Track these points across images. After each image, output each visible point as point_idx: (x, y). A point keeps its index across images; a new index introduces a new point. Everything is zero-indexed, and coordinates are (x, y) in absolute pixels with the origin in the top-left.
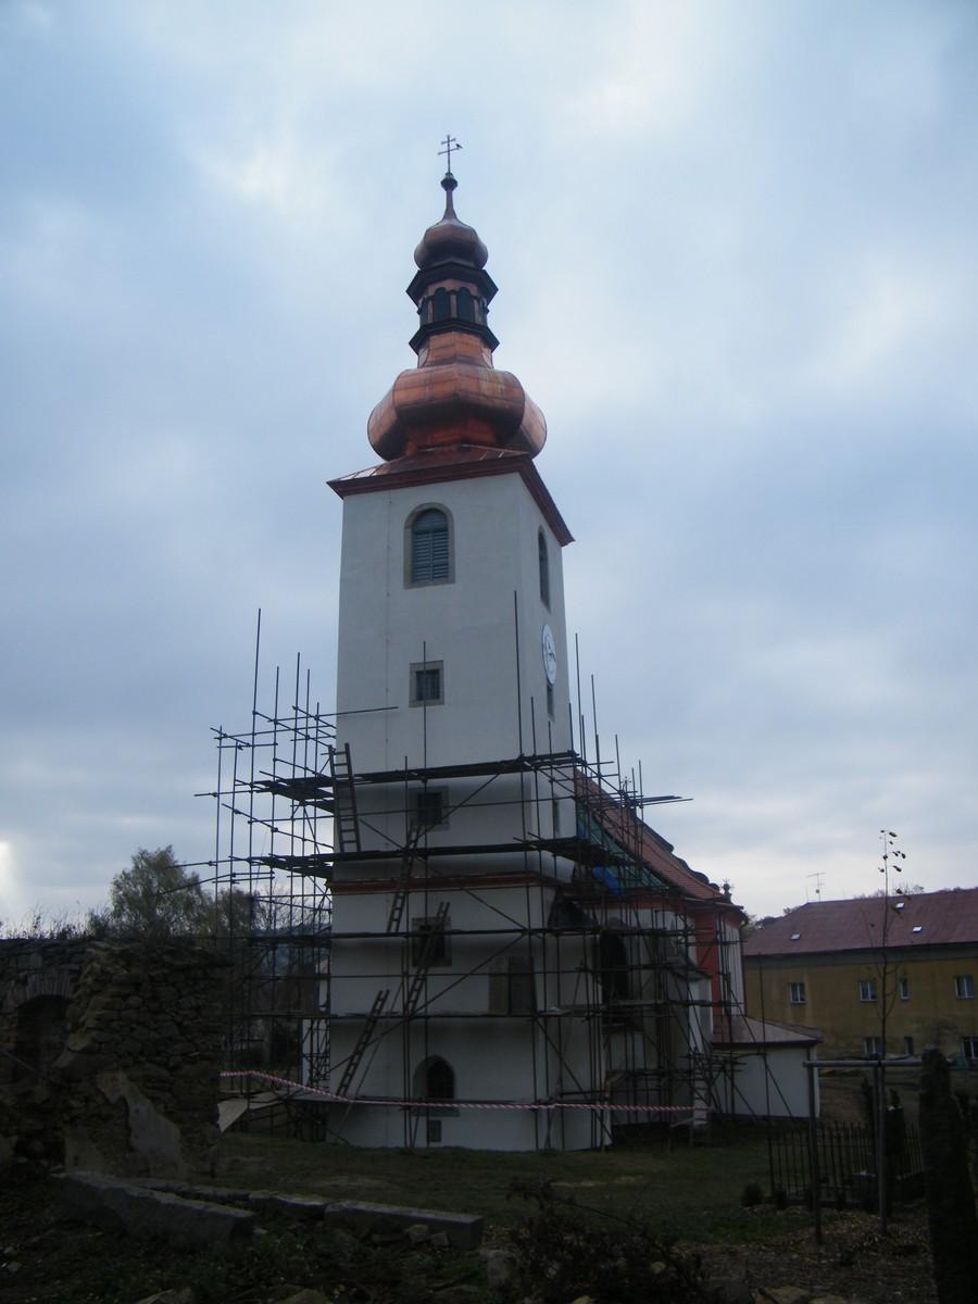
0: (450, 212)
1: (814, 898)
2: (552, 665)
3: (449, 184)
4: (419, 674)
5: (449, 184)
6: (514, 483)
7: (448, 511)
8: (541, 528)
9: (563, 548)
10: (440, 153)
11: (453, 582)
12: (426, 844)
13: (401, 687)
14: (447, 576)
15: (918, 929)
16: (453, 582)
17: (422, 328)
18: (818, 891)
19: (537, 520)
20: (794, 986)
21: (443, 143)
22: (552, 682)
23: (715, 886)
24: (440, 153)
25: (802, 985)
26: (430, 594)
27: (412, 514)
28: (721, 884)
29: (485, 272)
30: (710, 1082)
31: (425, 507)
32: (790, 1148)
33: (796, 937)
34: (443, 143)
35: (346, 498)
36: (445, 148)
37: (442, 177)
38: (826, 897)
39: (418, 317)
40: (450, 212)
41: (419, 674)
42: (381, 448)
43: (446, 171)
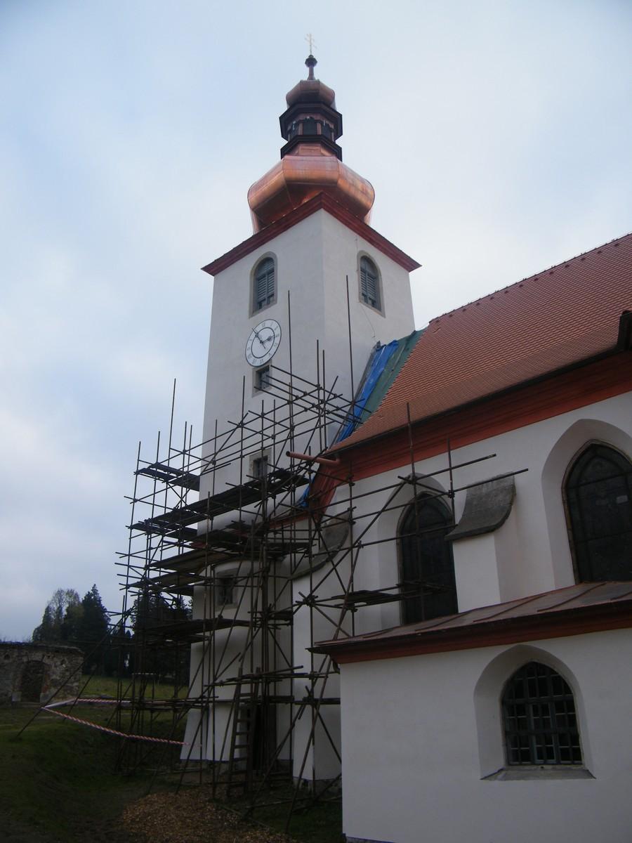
3: (311, 62)
5: (311, 62)
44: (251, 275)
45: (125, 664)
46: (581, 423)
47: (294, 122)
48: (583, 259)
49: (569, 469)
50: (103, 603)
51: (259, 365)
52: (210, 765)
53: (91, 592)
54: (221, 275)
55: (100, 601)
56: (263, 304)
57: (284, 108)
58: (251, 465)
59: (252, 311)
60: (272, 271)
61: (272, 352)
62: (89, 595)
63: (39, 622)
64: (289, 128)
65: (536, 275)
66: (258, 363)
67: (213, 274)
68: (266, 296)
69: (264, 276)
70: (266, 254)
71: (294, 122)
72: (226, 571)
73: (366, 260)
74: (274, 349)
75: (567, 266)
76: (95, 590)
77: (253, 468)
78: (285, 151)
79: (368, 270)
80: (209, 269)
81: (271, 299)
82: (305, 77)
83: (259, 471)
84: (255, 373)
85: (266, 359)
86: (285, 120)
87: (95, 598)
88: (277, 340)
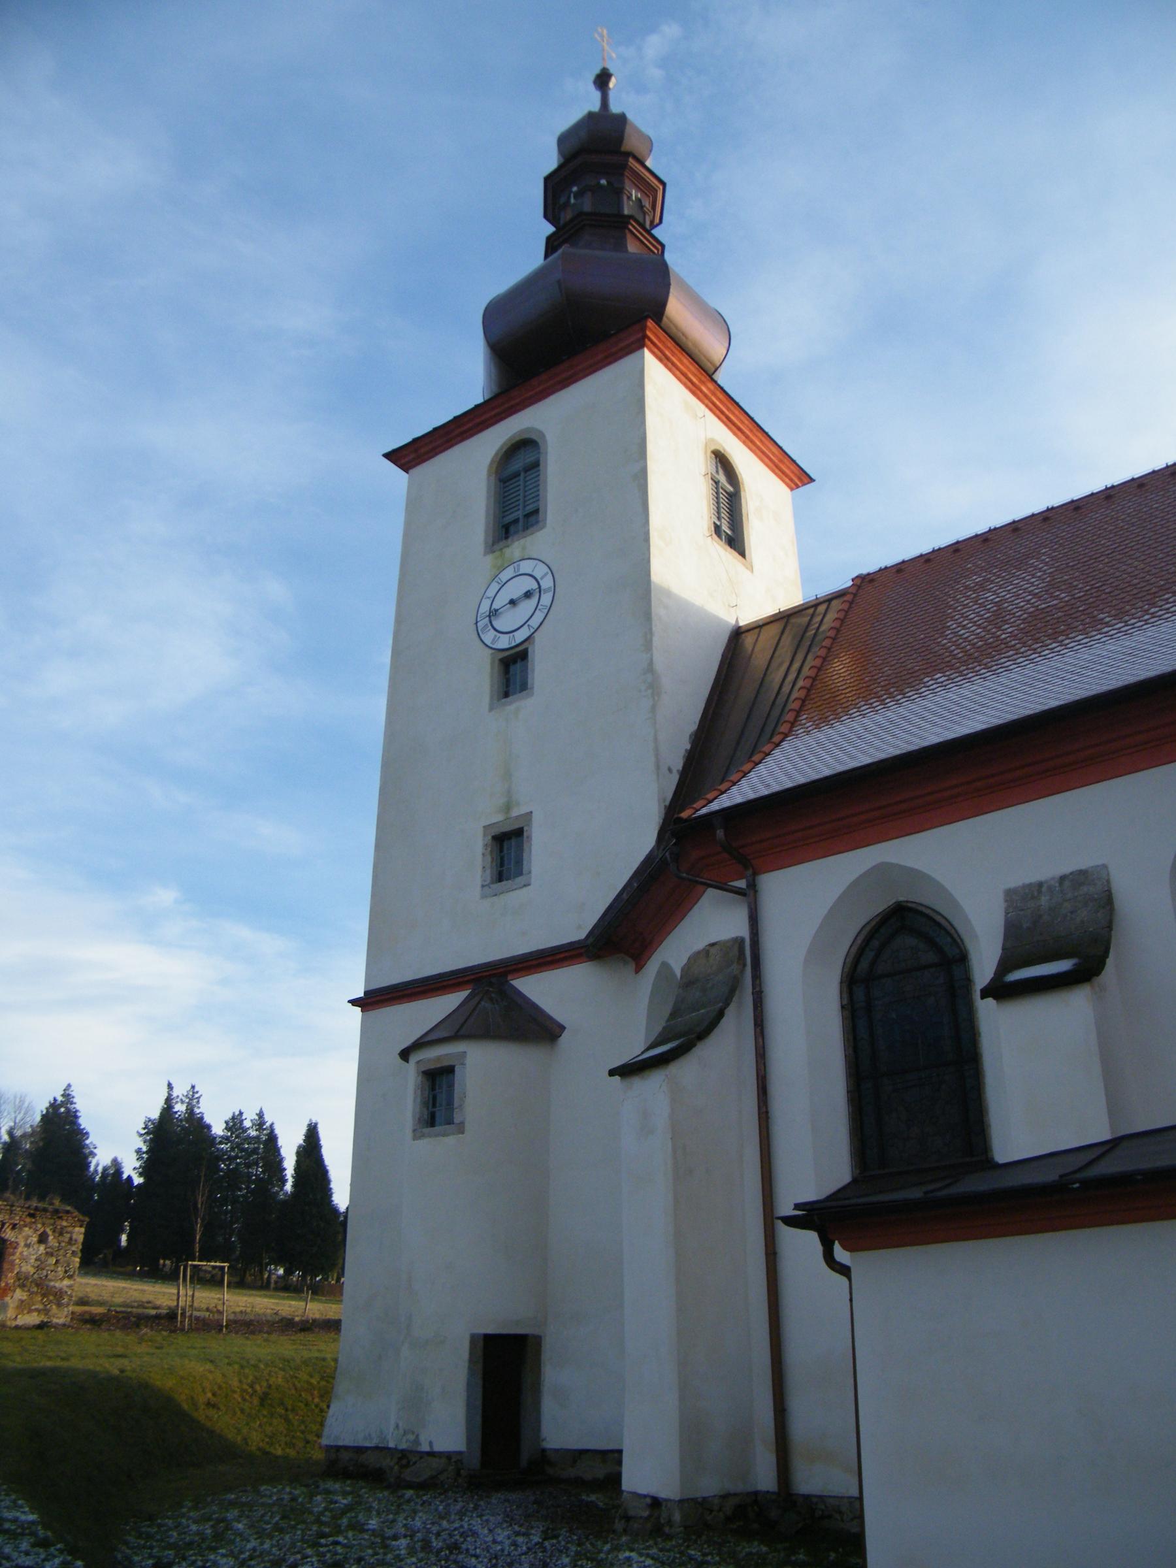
3: (602, 80)
5: (602, 80)
44: (489, 471)
45: (120, 1241)
46: (882, 871)
47: (575, 189)
48: (957, 551)
49: (854, 950)
50: (81, 1121)
51: (506, 646)
52: (400, 1459)
53: (60, 1099)
54: (413, 471)
55: (77, 1117)
56: (512, 529)
57: (551, 162)
58: (486, 845)
59: (490, 542)
60: (535, 466)
61: (535, 622)
62: (54, 1106)
63: (155, 1115)
64: (562, 200)
65: (1014, 522)
66: (504, 642)
67: (406, 468)
68: (520, 514)
69: (516, 475)
70: (523, 431)
71: (575, 189)
72: (439, 1058)
73: (722, 460)
74: (539, 616)
75: (1077, 509)
76: (67, 1096)
77: (491, 852)
78: (552, 245)
79: (722, 478)
80: (393, 456)
81: (532, 519)
82: (594, 105)
83: (502, 859)
84: (497, 662)
85: (520, 636)
86: (555, 186)
87: (68, 1111)
88: (546, 599)
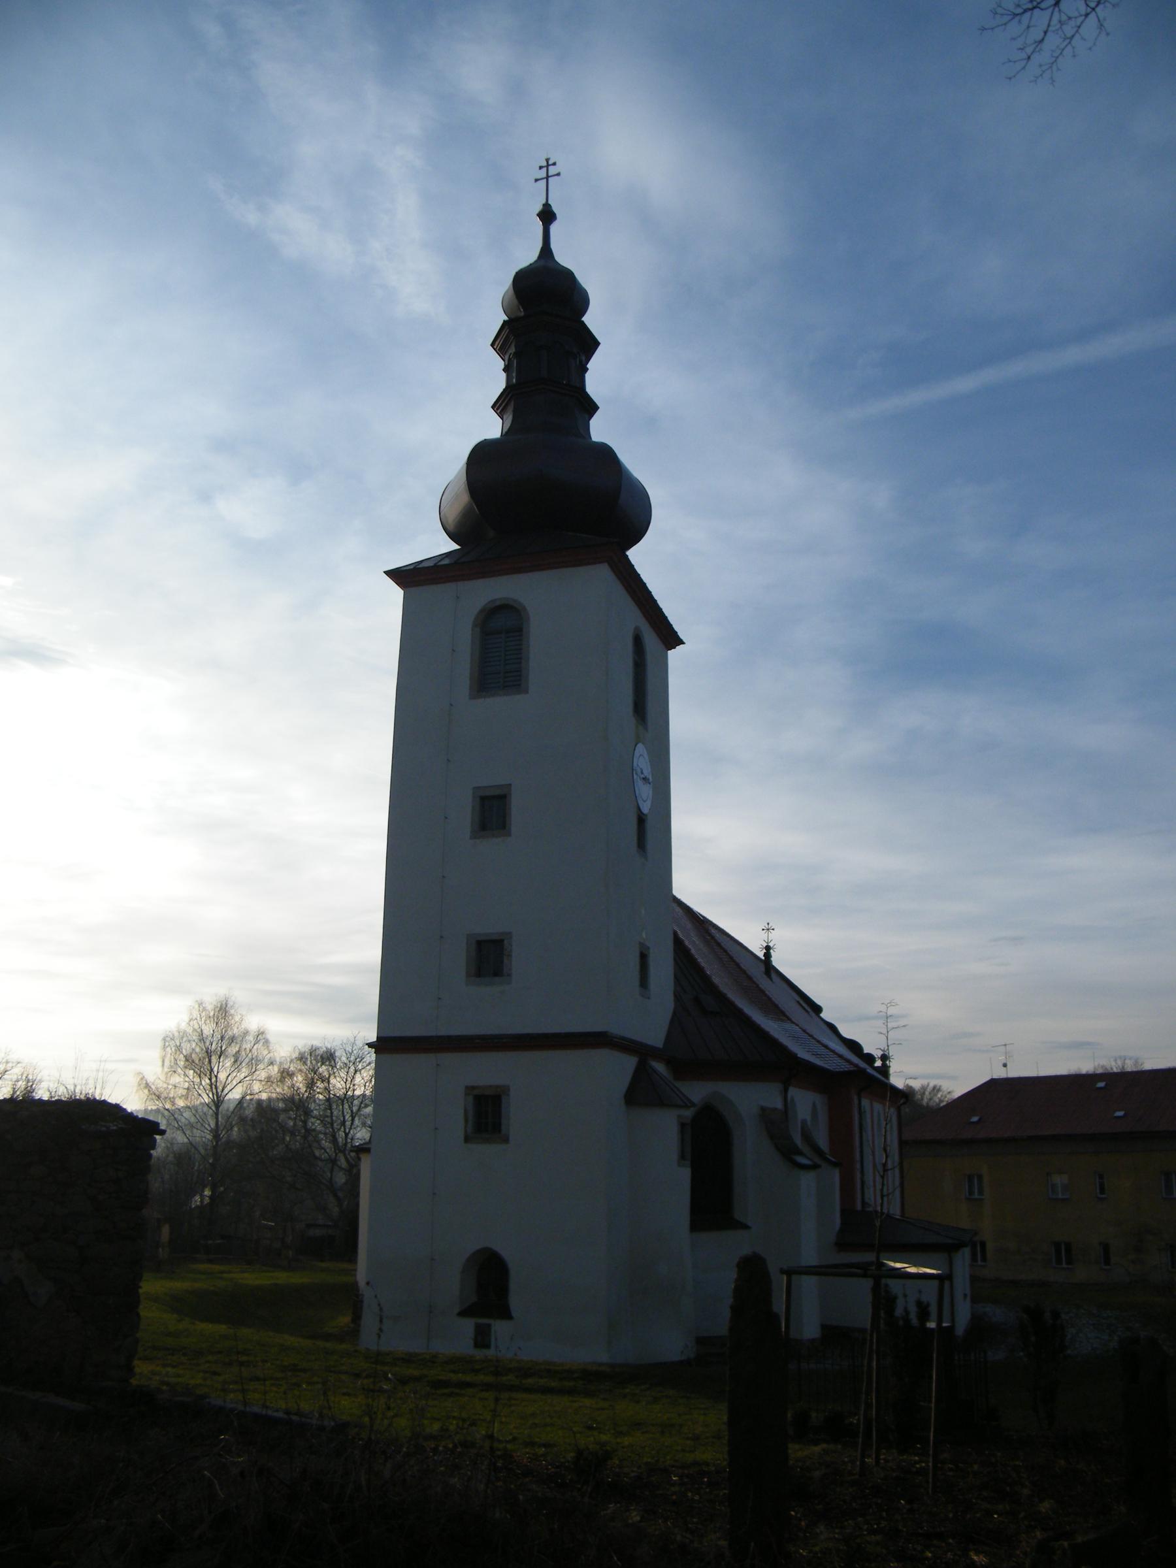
0: (546, 251)
1: (1000, 1073)
2: (645, 793)
3: (547, 216)
4: (483, 799)
5: (547, 216)
6: (602, 574)
7: (524, 609)
8: (637, 629)
9: (669, 651)
10: (536, 180)
11: (526, 692)
12: (1007, 1074)
13: (464, 814)
14: (519, 685)
15: (1120, 1113)
16: (526, 692)
17: (506, 387)
18: (1005, 1065)
19: (634, 618)
20: (970, 1178)
21: (541, 168)
22: (645, 810)
23: (870, 1059)
24: (536, 180)
25: (980, 1177)
26: (499, 704)
27: (481, 611)
28: (877, 1054)
29: (583, 322)
30: (346, 1144)
31: (498, 603)
32: (208, 1132)
33: (975, 1119)
34: (541, 168)
35: (413, 590)
36: (543, 173)
37: (538, 208)
38: (1014, 1072)
39: (504, 375)
40: (546, 251)
41: (483, 799)
42: (453, 536)
43: (544, 201)
